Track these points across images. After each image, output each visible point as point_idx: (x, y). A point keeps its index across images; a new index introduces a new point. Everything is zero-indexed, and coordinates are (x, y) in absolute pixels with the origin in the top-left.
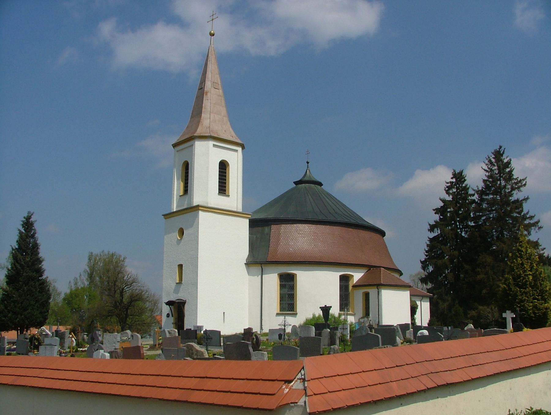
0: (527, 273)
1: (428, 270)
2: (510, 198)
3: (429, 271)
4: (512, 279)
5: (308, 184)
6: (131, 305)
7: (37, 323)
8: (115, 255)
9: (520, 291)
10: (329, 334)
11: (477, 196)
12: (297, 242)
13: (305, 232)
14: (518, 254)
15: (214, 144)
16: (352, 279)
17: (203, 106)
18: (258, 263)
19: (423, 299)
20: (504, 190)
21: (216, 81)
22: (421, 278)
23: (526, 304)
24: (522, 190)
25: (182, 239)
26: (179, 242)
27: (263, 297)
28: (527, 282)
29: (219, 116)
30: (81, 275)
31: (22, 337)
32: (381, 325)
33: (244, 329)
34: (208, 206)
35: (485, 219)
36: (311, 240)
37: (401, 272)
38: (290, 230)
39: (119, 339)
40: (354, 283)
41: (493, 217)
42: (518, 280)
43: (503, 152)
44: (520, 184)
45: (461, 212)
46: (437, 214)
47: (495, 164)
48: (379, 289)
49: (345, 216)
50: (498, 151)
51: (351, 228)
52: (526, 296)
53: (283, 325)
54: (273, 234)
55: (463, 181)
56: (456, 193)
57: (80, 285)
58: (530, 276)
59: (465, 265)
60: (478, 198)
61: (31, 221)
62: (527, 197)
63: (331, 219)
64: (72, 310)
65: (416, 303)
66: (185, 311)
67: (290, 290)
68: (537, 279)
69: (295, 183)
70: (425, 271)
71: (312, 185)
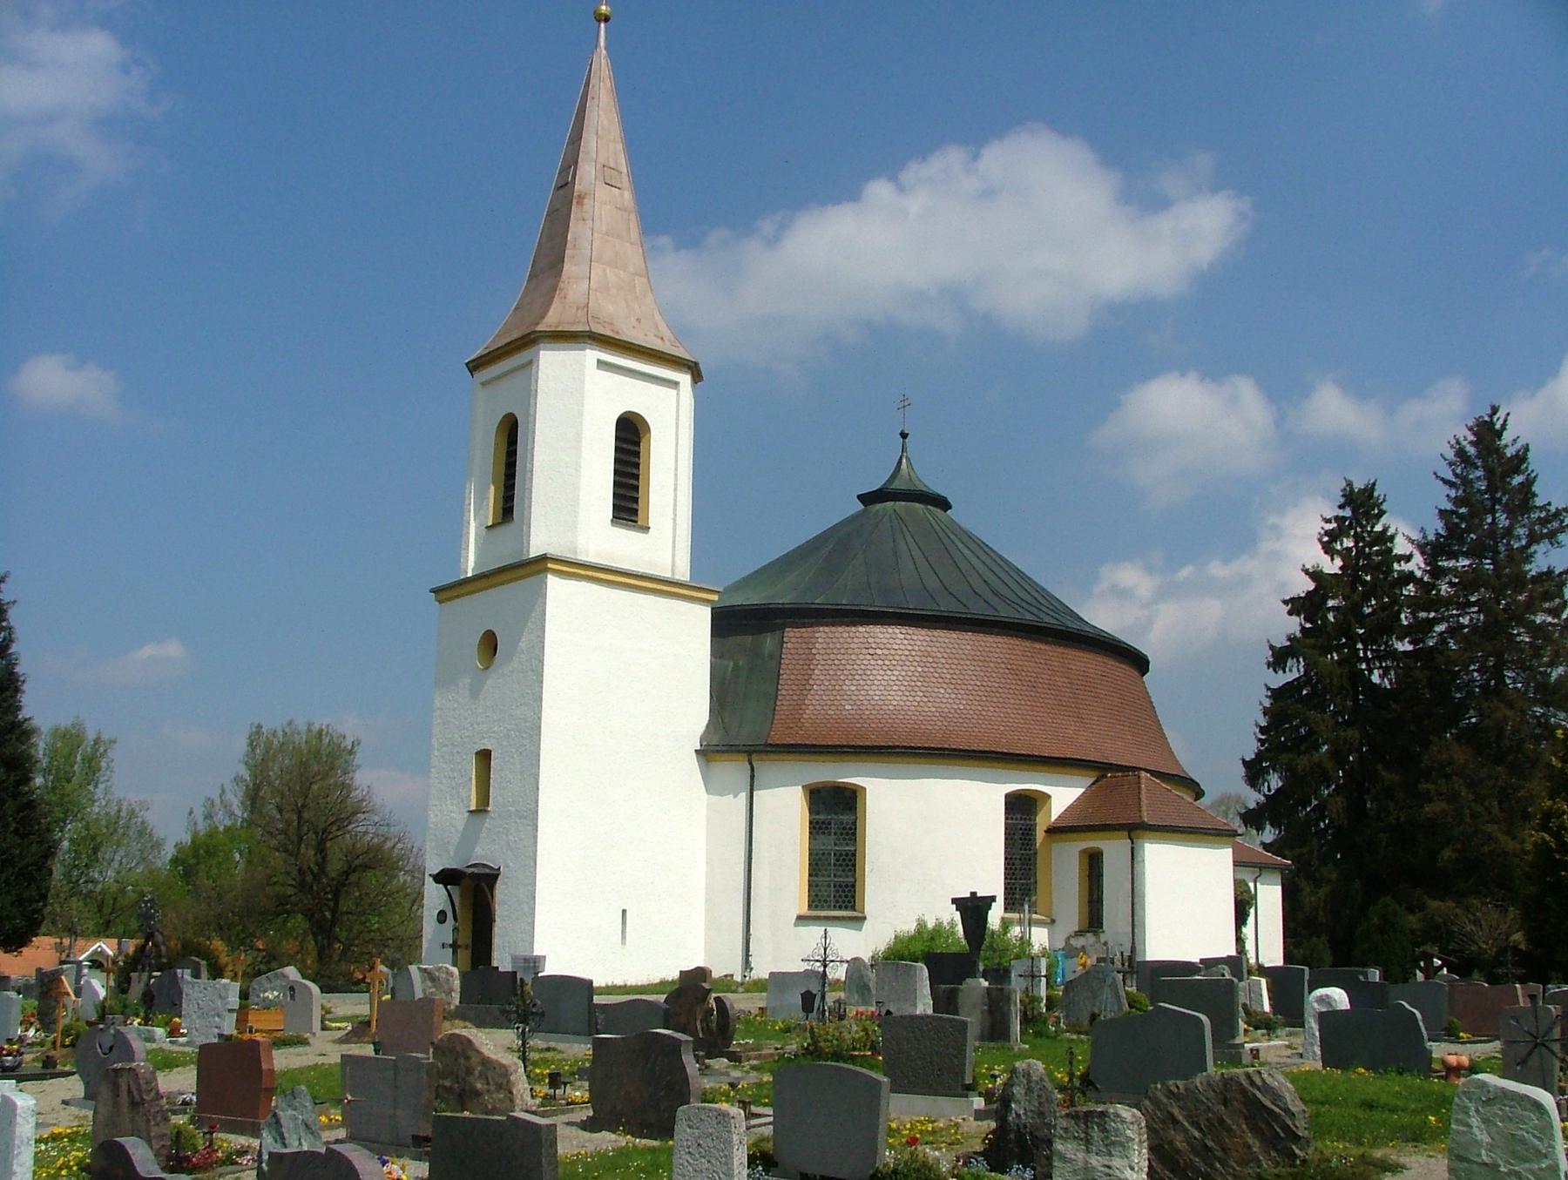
1: (1266, 784)
2: (1527, 567)
3: (1269, 790)
5: (903, 503)
6: (347, 882)
8: (327, 735)
10: (986, 1000)
11: (1422, 559)
12: (869, 682)
13: (893, 652)
17: (569, 238)
20: (1505, 541)
22: (1246, 812)
24: (1563, 543)
27: (753, 860)
30: (223, 791)
32: (1142, 960)
33: (681, 972)
34: (579, 558)
35: (1444, 632)
37: (1198, 785)
38: (846, 646)
40: (1054, 818)
45: (1370, 610)
46: (1293, 617)
47: (1476, 461)
48: (1134, 840)
49: (1024, 604)
50: (1486, 421)
51: (1042, 642)
53: (818, 961)
57: (222, 821)
59: (1383, 773)
60: (1423, 566)
63: (979, 609)
66: (496, 905)
67: (844, 839)
69: (861, 498)
71: (917, 505)
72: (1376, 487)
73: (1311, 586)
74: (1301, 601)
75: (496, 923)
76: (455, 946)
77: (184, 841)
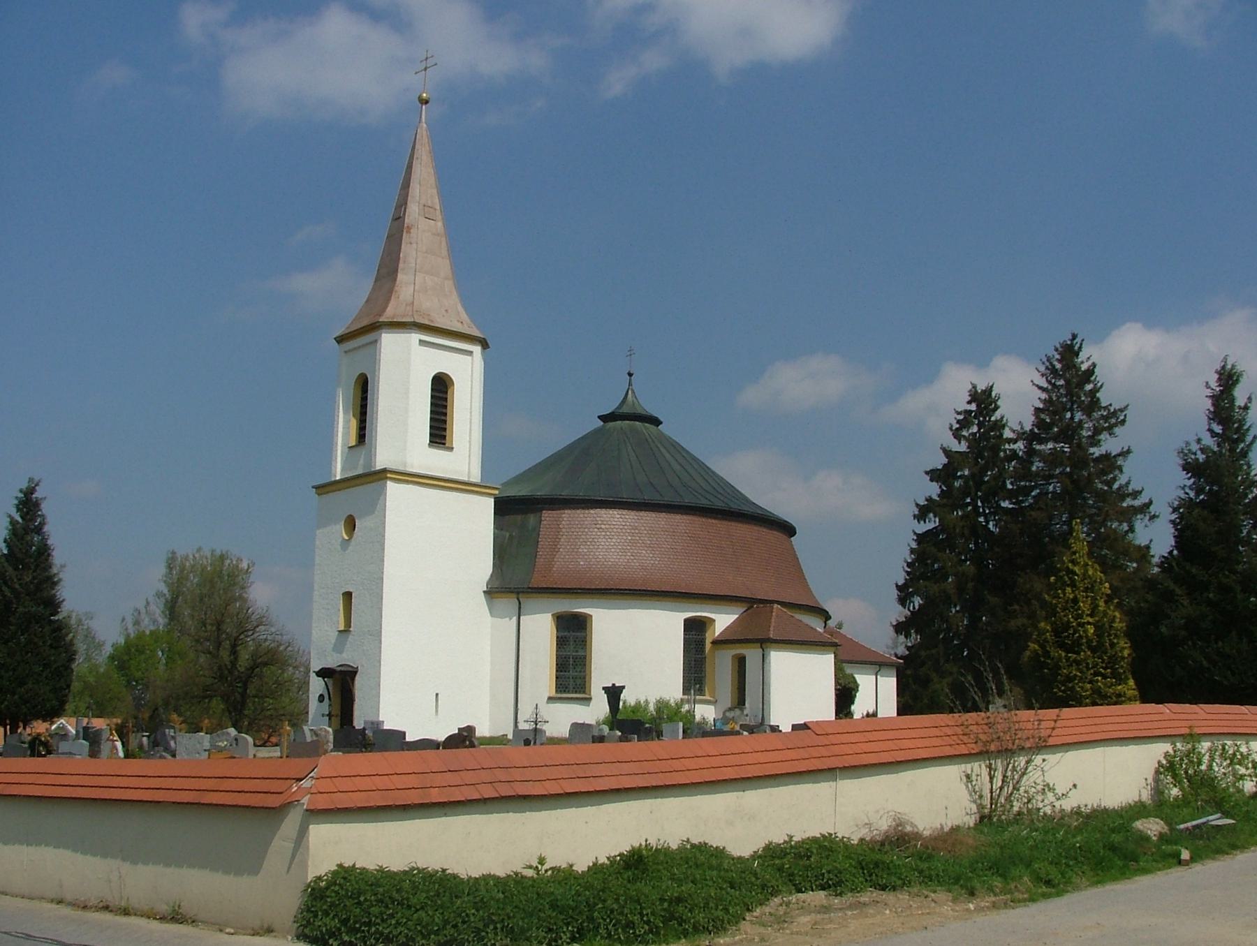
0: (1083, 621)
1: (912, 604)
3: (914, 608)
4: (1052, 632)
5: (628, 422)
6: (253, 675)
7: (45, 711)
9: (1068, 659)
13: (612, 527)
14: (1067, 579)
15: (422, 339)
16: (712, 627)
18: (512, 590)
19: (882, 670)
21: (430, 204)
23: (1077, 687)
25: (353, 539)
26: (345, 544)
28: (1082, 639)
29: (436, 279)
30: (148, 603)
31: (13, 740)
36: (626, 544)
37: (828, 612)
39: (207, 745)
40: (717, 634)
41: (1054, 492)
42: (1063, 633)
43: (1080, 348)
44: (1113, 421)
51: (715, 518)
52: (1076, 670)
54: (545, 529)
55: (994, 408)
56: (978, 435)
57: (147, 626)
58: (1089, 626)
59: (988, 597)
61: (36, 498)
62: (1127, 448)
64: (129, 682)
65: (854, 678)
68: (1104, 633)
70: (905, 608)
71: (637, 423)
72: (993, 389)
73: (945, 460)
74: (938, 472)
75: (356, 702)
76: (330, 715)
77: (119, 642)
